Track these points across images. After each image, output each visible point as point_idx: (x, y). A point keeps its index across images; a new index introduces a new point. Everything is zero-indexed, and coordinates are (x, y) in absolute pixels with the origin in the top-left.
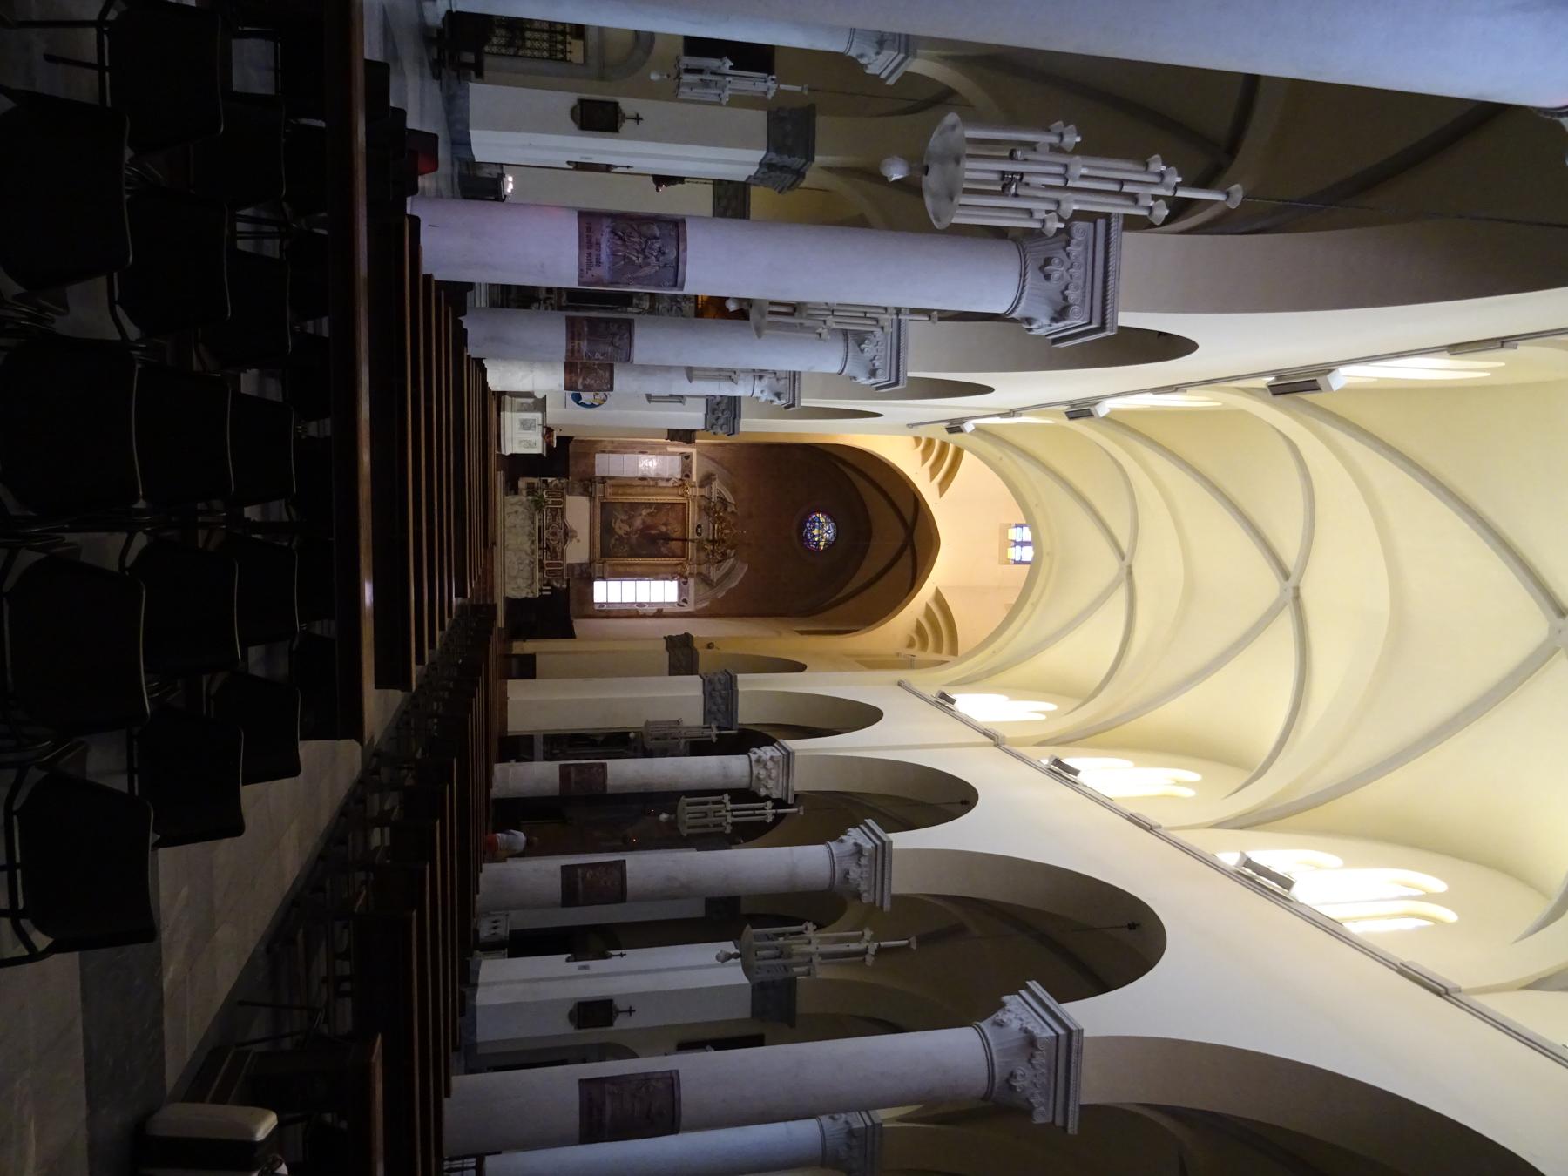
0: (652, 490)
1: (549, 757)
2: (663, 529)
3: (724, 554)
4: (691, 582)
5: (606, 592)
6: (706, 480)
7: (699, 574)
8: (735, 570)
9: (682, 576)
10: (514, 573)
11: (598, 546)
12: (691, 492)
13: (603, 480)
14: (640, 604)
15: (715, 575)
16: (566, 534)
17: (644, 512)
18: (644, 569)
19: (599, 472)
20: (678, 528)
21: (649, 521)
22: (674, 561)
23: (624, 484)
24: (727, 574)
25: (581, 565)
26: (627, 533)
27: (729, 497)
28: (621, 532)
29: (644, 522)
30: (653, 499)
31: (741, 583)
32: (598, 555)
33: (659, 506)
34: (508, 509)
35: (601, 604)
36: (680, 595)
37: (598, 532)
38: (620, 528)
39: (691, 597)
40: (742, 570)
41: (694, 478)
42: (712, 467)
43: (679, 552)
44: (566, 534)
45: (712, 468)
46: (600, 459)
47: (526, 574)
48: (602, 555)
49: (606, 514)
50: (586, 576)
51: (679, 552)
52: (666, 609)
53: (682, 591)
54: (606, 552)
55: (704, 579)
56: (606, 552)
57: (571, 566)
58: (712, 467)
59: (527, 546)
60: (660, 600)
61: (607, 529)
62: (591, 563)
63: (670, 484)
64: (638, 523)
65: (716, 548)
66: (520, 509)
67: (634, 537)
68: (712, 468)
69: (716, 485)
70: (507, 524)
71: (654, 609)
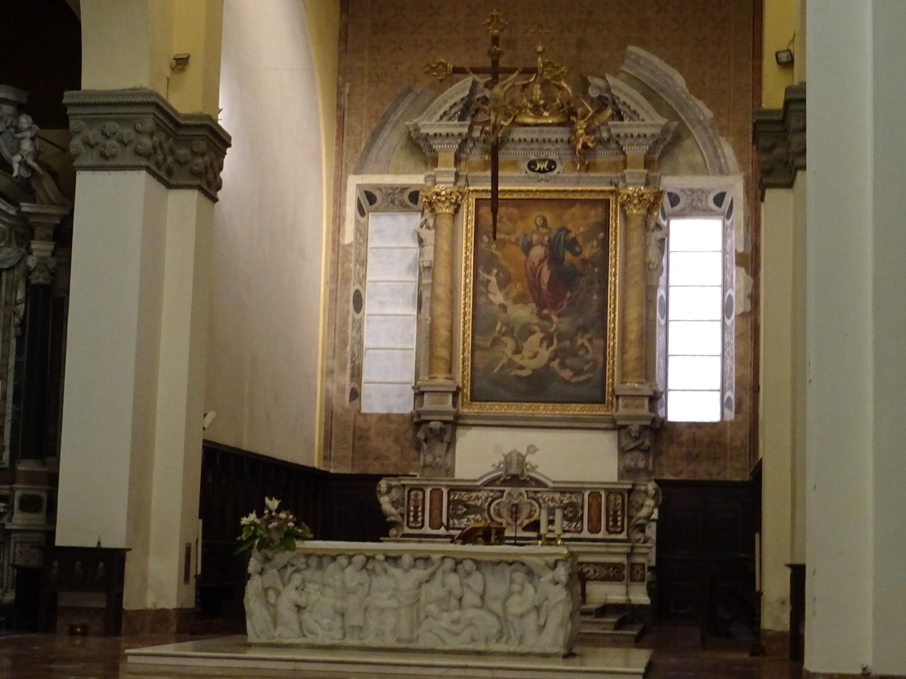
0: (443, 275)
1: (554, 514)
2: (538, 252)
3: (601, 103)
4: (670, 183)
5: (694, 392)
6: (420, 149)
7: (648, 164)
8: (645, 77)
9: (653, 205)
10: (490, 624)
11: (575, 410)
12: (445, 184)
13: (419, 394)
14: (726, 310)
15: (652, 122)
16: (515, 480)
17: (498, 297)
18: (634, 294)
19: (404, 405)
20: (535, 216)
21: (518, 288)
22: (616, 223)
23: (432, 348)
24: (651, 95)
25: (622, 452)
26: (548, 339)
27: (460, 89)
28: (545, 354)
29: (520, 299)
30: (465, 278)
31: (678, 65)
32: (598, 410)
33: (482, 261)
34: (288, 633)
35: (724, 404)
36: (706, 213)
37: (543, 410)
38: (535, 355)
39: (711, 183)
40: (646, 61)
41: (416, 179)
42: (392, 139)
43: (595, 215)
44: (515, 480)
45: (393, 138)
46: (375, 402)
47: (497, 587)
48: (601, 401)
49: (504, 389)
50: (652, 435)
51: (595, 215)
52: (738, 243)
53: (695, 210)
54: (596, 393)
55: (664, 149)
56: (596, 393)
57: (626, 472)
58: (392, 139)
59: (405, 579)
60: (717, 260)
61: (536, 387)
62: (618, 427)
63: (429, 235)
64: (523, 313)
65: (586, 120)
66: (290, 595)
67: (559, 323)
68: (393, 138)
69: (429, 125)
70: (335, 637)
71: (738, 275)
